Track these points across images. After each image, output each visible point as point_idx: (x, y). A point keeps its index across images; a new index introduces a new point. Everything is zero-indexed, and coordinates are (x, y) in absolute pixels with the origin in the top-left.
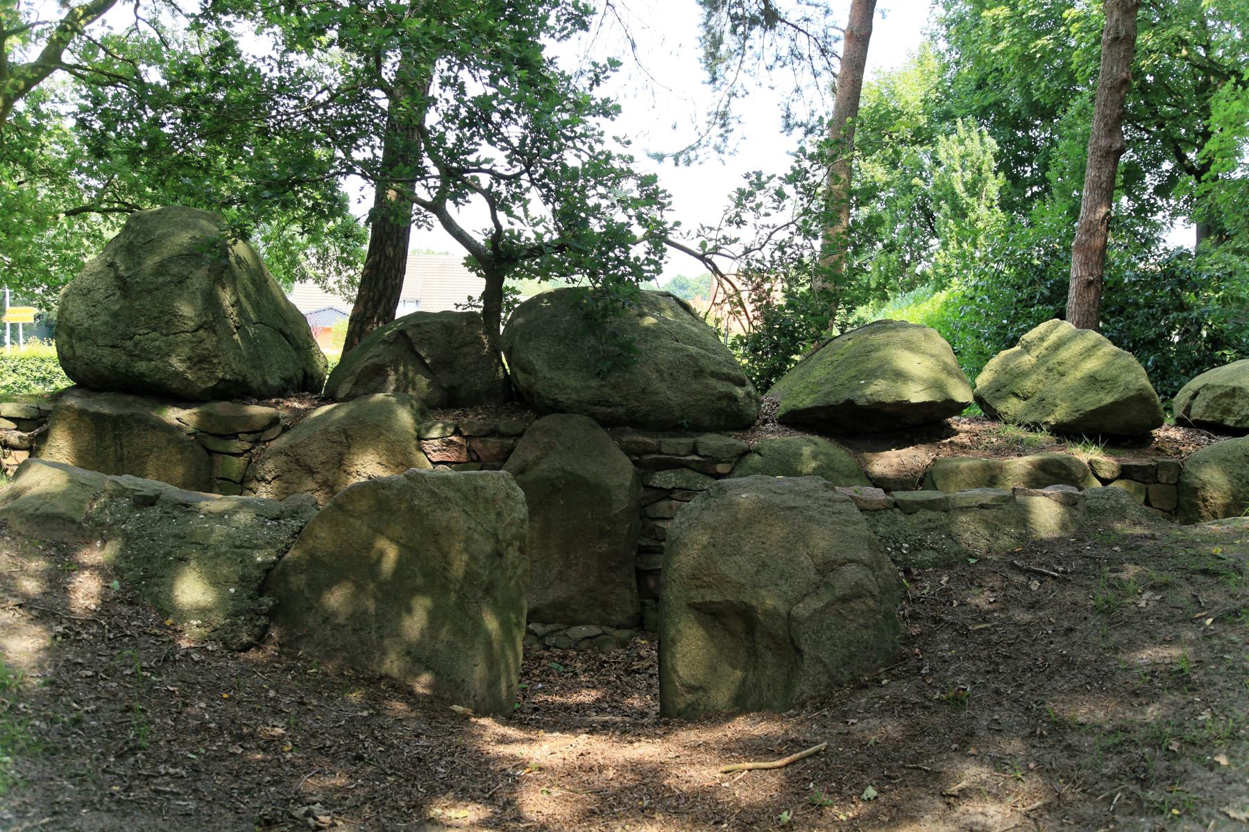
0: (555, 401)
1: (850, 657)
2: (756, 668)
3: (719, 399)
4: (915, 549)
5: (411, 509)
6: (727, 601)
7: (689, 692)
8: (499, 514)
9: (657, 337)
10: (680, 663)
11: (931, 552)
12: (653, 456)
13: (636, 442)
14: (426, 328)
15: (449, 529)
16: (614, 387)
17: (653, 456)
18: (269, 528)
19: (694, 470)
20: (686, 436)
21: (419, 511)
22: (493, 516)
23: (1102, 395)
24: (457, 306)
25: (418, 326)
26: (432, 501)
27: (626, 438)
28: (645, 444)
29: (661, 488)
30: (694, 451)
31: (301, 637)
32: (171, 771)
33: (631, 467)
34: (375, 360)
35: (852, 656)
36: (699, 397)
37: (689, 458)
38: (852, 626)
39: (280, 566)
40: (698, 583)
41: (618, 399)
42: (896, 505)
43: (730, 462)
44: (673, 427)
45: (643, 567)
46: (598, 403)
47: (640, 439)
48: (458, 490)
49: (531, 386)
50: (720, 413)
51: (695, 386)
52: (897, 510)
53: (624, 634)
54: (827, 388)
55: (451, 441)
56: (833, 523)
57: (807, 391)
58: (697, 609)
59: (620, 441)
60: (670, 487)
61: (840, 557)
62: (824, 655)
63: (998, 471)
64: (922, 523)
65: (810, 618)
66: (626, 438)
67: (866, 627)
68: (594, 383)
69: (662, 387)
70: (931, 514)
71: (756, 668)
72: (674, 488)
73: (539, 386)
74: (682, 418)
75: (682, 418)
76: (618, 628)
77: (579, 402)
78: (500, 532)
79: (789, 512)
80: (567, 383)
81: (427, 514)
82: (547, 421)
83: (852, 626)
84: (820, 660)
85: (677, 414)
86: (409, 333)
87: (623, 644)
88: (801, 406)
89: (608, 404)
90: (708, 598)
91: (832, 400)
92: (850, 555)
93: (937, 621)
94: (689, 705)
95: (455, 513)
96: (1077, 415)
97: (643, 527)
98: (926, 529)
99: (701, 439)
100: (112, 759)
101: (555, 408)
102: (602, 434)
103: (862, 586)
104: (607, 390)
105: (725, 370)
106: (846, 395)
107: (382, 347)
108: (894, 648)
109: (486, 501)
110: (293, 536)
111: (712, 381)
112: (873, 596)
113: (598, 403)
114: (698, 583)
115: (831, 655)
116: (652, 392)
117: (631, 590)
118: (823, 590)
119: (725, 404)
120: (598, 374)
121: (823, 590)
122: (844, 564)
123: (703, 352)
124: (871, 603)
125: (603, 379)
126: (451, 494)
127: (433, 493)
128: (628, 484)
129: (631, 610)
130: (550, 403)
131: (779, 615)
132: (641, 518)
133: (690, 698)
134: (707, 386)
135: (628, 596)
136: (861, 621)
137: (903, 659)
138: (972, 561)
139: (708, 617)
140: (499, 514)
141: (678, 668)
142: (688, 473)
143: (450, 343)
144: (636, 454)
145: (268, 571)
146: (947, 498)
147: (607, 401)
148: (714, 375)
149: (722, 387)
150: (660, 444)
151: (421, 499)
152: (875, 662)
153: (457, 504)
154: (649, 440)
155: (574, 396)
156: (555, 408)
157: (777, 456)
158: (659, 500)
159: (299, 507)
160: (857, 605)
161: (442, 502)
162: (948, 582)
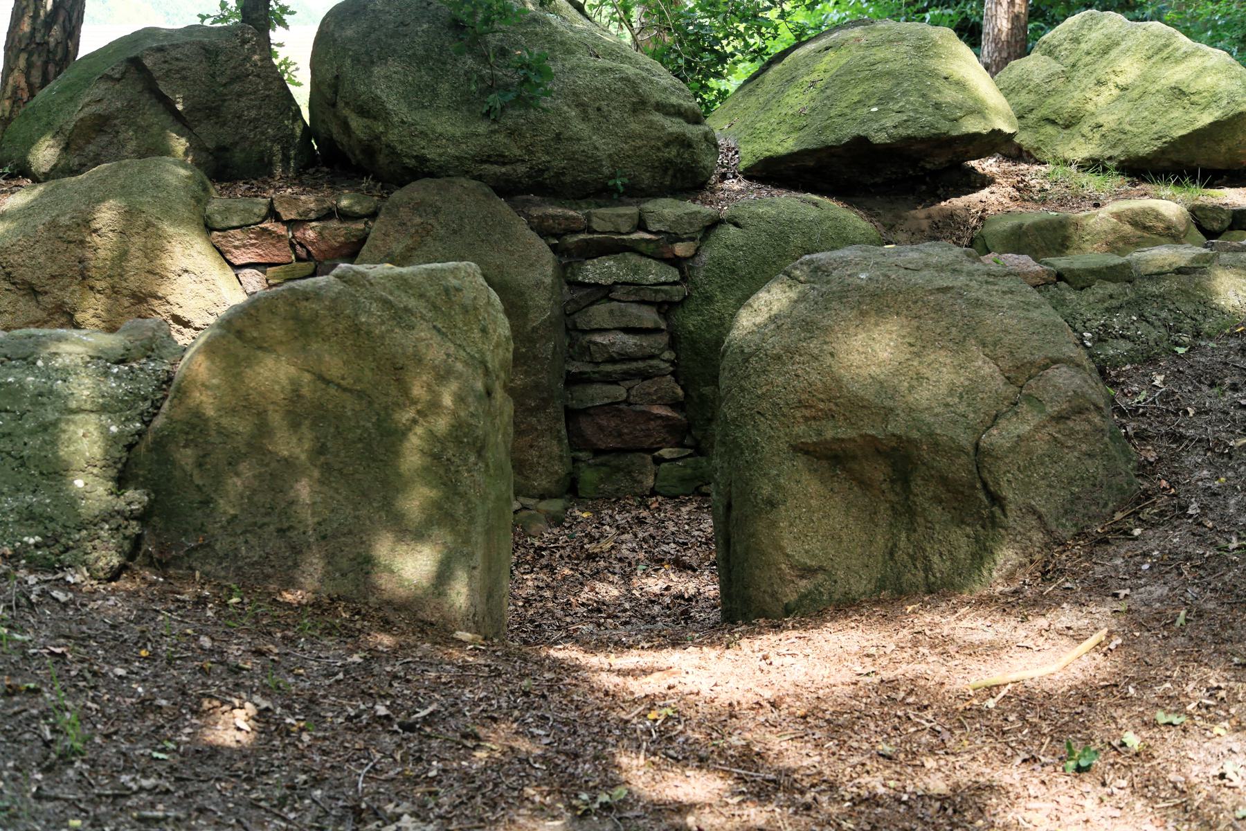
0: (422, 160)
1: (1072, 502)
2: (911, 529)
3: (667, 145)
4: (1100, 340)
5: (356, 329)
6: (864, 436)
7: (802, 577)
8: (484, 331)
9: (570, 52)
10: (786, 534)
11: (1122, 342)
12: (582, 236)
13: (554, 217)
14: (174, 53)
15: (419, 360)
16: (511, 133)
17: (582, 236)
18: (117, 376)
19: (642, 254)
20: (623, 204)
21: (368, 333)
22: (476, 334)
23: (1195, 114)
24: (203, 18)
25: (161, 49)
26: (386, 315)
27: (536, 212)
28: (567, 218)
29: (596, 284)
30: (641, 226)
31: (194, 549)
32: (146, 783)
33: (549, 255)
34: (94, 109)
35: (1076, 498)
36: (639, 143)
37: (635, 236)
38: (1072, 457)
39: (149, 438)
40: (807, 413)
41: (517, 152)
42: (1060, 277)
43: (692, 239)
44: (603, 193)
45: (574, 404)
46: (488, 160)
47: (559, 211)
48: (422, 296)
49: (378, 138)
50: (666, 165)
51: (635, 126)
52: (1063, 285)
53: (556, 505)
54: (818, 122)
55: (265, 230)
56: (1011, 307)
57: (784, 128)
58: (807, 453)
59: (528, 216)
60: (610, 281)
61: (1039, 357)
62: (1037, 503)
63: (1072, 230)
64: (1102, 301)
65: (1012, 450)
66: (536, 212)
67: (1091, 455)
68: (482, 128)
69: (579, 127)
70: (1111, 288)
71: (911, 529)
72: (615, 283)
73: (393, 136)
74: (613, 176)
75: (613, 176)
76: (542, 497)
77: (458, 158)
78: (489, 357)
79: (940, 296)
80: (439, 129)
81: (382, 337)
82: (416, 191)
83: (1072, 457)
84: (1033, 511)
85: (606, 171)
86: (148, 62)
87: (556, 521)
88: (781, 150)
89: (502, 160)
90: (829, 434)
91: (830, 138)
92: (1053, 353)
93: (1177, 438)
94: (804, 596)
95: (423, 332)
96: (1159, 144)
97: (571, 345)
98: (1107, 310)
99: (649, 206)
100: (39, 776)
101: (420, 170)
102: (502, 206)
103: (1083, 395)
104: (501, 138)
105: (674, 100)
106: (850, 131)
107: (103, 86)
108: (1130, 484)
109: (465, 310)
110: (159, 388)
111: (658, 118)
112: (1098, 409)
113: (488, 160)
114: (807, 413)
115: (1047, 500)
116: (570, 139)
117: (560, 441)
118: (1024, 407)
119: (674, 152)
120: (488, 114)
121: (1024, 407)
122: (1046, 367)
123: (644, 74)
124: (1097, 419)
125: (495, 121)
126: (412, 303)
127: (386, 303)
128: (548, 281)
129: (560, 469)
130: (411, 163)
131: (961, 450)
132: (568, 330)
133: (804, 585)
134: (651, 125)
135: (556, 450)
136: (1084, 447)
137: (1148, 498)
138: (1181, 351)
139: (825, 463)
140: (484, 331)
141: (784, 543)
142: (634, 259)
143: (213, 76)
144: (555, 236)
145: (130, 447)
146: (1129, 262)
147: (502, 156)
148: (661, 108)
149: (674, 126)
150: (588, 217)
151: (370, 314)
152: (1105, 505)
153: (423, 318)
154: (572, 213)
155: (452, 150)
156: (420, 170)
157: (763, 225)
158: (592, 304)
159: (151, 339)
160: (1078, 424)
161: (401, 316)
162: (1164, 383)
